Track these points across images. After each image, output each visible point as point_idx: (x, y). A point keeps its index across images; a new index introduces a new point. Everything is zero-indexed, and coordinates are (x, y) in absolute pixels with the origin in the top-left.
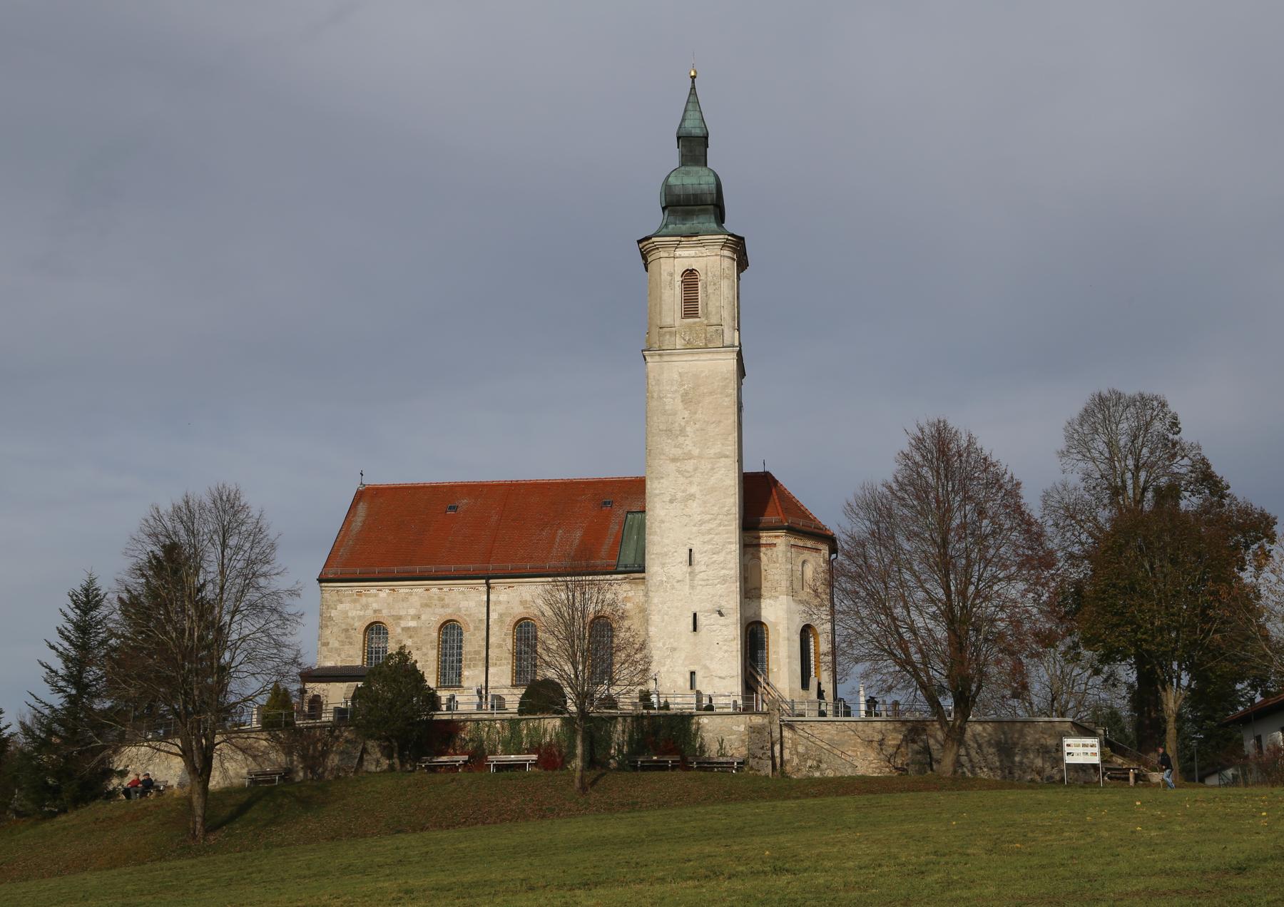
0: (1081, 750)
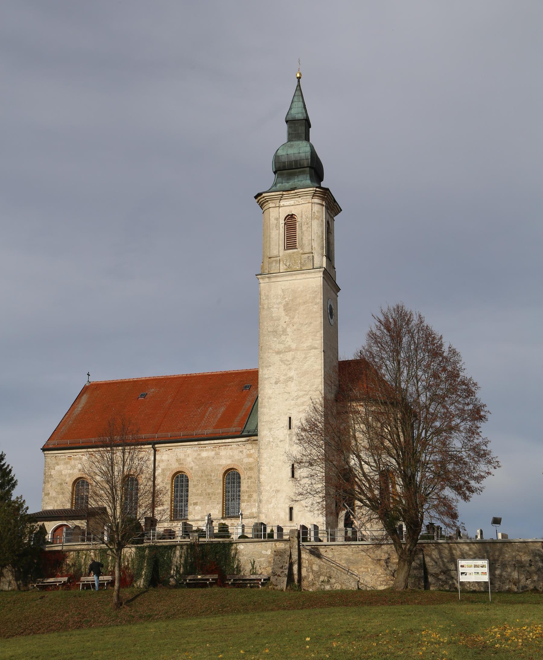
0: (473, 570)
